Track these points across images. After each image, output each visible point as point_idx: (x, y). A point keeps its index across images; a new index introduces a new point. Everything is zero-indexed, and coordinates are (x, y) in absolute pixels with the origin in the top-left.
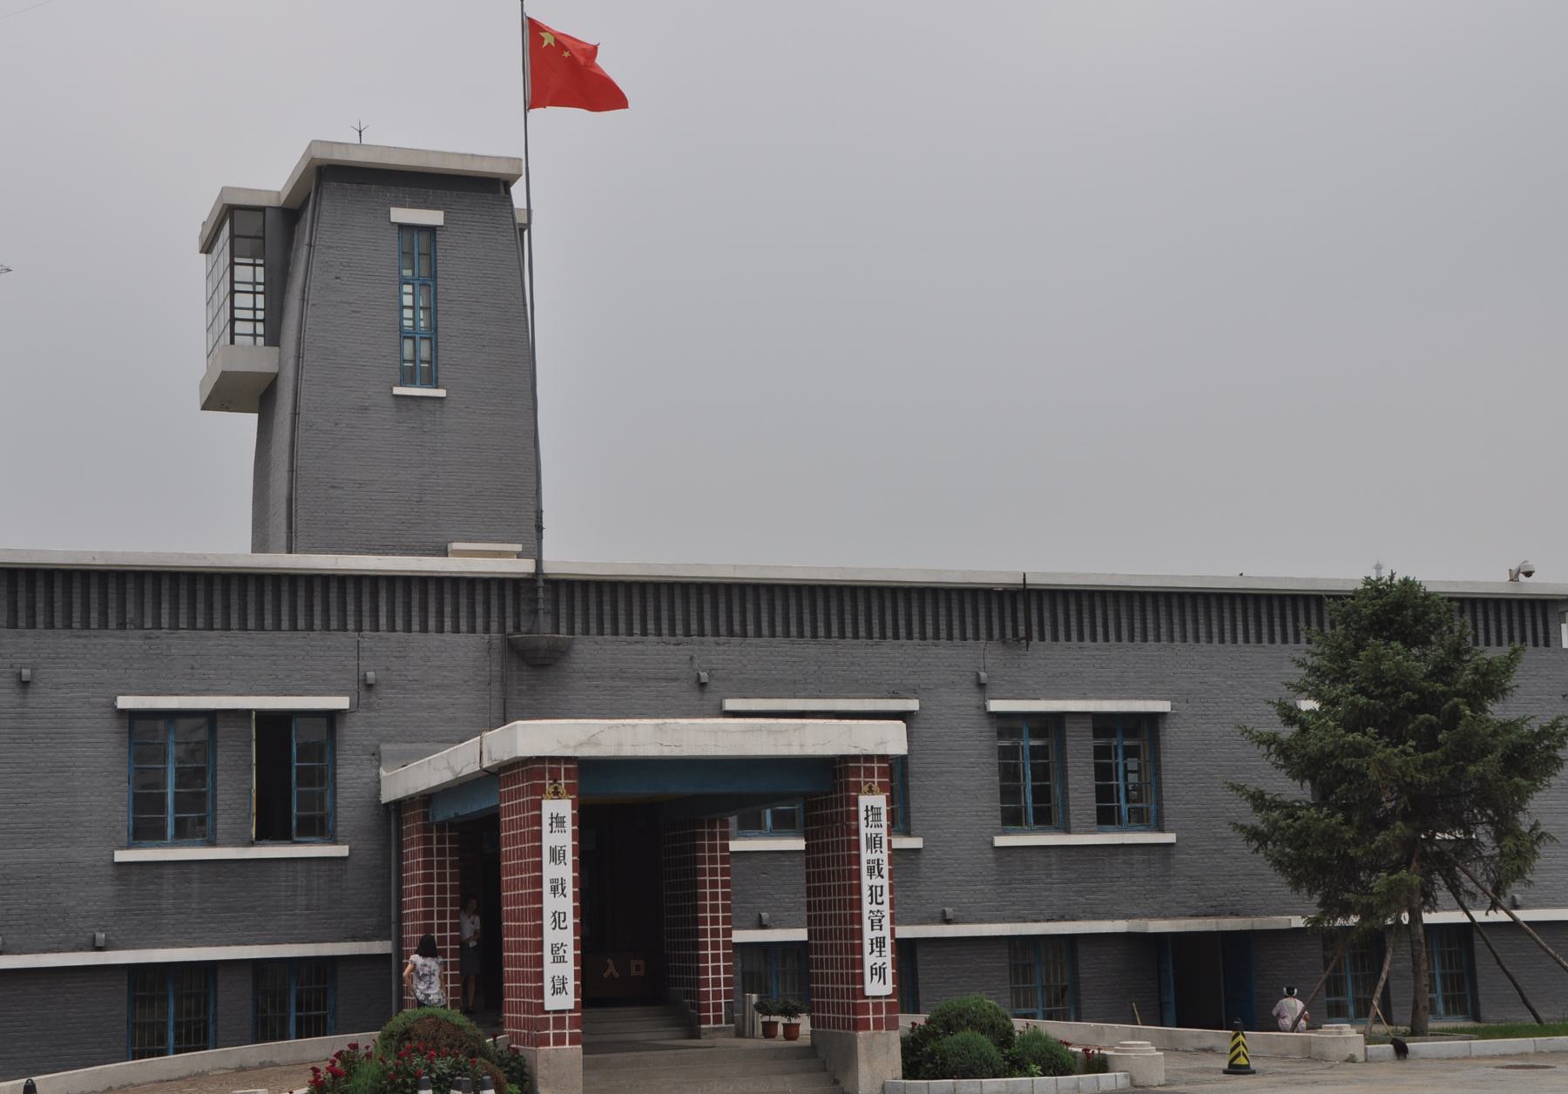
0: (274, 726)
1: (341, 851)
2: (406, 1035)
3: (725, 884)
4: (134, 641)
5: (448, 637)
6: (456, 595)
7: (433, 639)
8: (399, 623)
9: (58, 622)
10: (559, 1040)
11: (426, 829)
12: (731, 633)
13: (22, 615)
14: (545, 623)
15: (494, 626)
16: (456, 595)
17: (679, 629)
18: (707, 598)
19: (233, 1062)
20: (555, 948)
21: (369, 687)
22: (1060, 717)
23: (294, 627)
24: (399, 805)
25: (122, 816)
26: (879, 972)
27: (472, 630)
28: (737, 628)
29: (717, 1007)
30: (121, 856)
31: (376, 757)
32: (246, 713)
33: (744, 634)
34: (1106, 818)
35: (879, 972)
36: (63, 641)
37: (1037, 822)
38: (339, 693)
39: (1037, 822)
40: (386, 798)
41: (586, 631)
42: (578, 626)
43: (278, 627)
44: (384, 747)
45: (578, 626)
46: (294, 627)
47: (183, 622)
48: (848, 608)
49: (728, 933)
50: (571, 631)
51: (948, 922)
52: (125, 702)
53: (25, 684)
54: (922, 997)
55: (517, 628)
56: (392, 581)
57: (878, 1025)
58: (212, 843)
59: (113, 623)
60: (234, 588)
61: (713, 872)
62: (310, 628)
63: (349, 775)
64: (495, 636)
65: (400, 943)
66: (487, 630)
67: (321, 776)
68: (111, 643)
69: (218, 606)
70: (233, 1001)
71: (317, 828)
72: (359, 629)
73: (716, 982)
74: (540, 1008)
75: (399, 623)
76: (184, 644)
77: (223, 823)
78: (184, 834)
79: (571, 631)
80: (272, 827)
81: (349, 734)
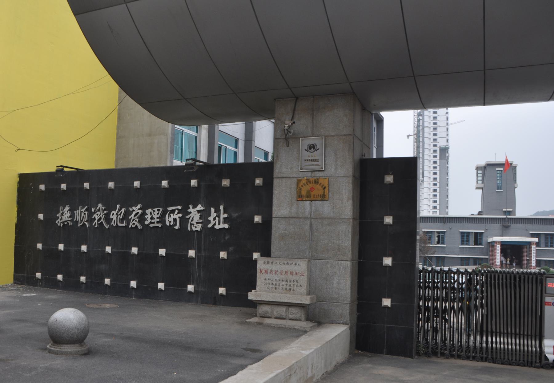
0: (476, 233)
1: (483, 247)
2: (483, 266)
3: (526, 253)
4: (461, 224)
5: (496, 224)
6: (451, 219)
7: (494, 224)
8: (490, 223)
9: (454, 222)
10: (498, 267)
11: (491, 245)
12: (531, 224)
13: (450, 222)
14: (507, 223)
15: (501, 223)
16: (451, 219)
17: (524, 223)
18: (448, 219)
19: (470, 267)
20: (498, 259)
21: (487, 230)
22: (540, 234)
23: (489, 223)
24: (489, 243)
25: (460, 242)
26: (534, 263)
27: (499, 223)
28: (532, 223)
29: (525, 266)
30: (460, 246)
31: (487, 237)
32: (472, 232)
33: (533, 224)
34: (547, 246)
35: (534, 263)
36: (454, 224)
37: (441, 243)
38: (483, 230)
39: (441, 243)
40: (488, 241)
41: (512, 224)
42: (512, 223)
43: (477, 223)
44: (488, 236)
45: (512, 223)
46: (478, 223)
47: (472, 223)
48: (439, 220)
49: (526, 258)
50: (511, 224)
51: (448, 255)
52: (460, 231)
53: (450, 229)
54: (541, 265)
55: (504, 223)
56: (499, 218)
57: (533, 268)
58: (469, 245)
59: (459, 222)
60: (452, 219)
61: (525, 251)
62: (480, 223)
63: (484, 239)
64: (501, 224)
65: (489, 257)
66: (500, 223)
67: (481, 239)
68: (459, 225)
69: (496, 221)
70: (471, 261)
71: (481, 244)
72: (486, 223)
73: (525, 263)
74: (531, 265)
75: (490, 223)
76: (470, 225)
77: (470, 243)
78: (467, 244)
79: (511, 224)
80: (476, 244)
81: (484, 235)
